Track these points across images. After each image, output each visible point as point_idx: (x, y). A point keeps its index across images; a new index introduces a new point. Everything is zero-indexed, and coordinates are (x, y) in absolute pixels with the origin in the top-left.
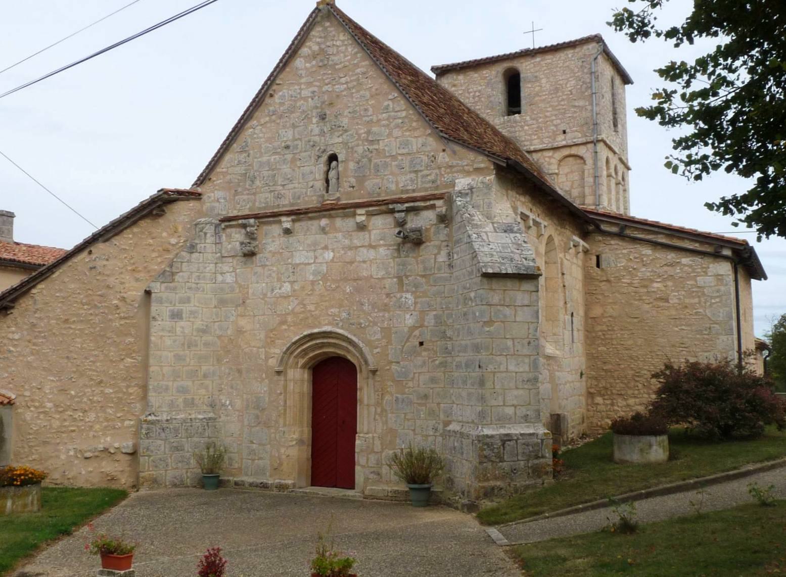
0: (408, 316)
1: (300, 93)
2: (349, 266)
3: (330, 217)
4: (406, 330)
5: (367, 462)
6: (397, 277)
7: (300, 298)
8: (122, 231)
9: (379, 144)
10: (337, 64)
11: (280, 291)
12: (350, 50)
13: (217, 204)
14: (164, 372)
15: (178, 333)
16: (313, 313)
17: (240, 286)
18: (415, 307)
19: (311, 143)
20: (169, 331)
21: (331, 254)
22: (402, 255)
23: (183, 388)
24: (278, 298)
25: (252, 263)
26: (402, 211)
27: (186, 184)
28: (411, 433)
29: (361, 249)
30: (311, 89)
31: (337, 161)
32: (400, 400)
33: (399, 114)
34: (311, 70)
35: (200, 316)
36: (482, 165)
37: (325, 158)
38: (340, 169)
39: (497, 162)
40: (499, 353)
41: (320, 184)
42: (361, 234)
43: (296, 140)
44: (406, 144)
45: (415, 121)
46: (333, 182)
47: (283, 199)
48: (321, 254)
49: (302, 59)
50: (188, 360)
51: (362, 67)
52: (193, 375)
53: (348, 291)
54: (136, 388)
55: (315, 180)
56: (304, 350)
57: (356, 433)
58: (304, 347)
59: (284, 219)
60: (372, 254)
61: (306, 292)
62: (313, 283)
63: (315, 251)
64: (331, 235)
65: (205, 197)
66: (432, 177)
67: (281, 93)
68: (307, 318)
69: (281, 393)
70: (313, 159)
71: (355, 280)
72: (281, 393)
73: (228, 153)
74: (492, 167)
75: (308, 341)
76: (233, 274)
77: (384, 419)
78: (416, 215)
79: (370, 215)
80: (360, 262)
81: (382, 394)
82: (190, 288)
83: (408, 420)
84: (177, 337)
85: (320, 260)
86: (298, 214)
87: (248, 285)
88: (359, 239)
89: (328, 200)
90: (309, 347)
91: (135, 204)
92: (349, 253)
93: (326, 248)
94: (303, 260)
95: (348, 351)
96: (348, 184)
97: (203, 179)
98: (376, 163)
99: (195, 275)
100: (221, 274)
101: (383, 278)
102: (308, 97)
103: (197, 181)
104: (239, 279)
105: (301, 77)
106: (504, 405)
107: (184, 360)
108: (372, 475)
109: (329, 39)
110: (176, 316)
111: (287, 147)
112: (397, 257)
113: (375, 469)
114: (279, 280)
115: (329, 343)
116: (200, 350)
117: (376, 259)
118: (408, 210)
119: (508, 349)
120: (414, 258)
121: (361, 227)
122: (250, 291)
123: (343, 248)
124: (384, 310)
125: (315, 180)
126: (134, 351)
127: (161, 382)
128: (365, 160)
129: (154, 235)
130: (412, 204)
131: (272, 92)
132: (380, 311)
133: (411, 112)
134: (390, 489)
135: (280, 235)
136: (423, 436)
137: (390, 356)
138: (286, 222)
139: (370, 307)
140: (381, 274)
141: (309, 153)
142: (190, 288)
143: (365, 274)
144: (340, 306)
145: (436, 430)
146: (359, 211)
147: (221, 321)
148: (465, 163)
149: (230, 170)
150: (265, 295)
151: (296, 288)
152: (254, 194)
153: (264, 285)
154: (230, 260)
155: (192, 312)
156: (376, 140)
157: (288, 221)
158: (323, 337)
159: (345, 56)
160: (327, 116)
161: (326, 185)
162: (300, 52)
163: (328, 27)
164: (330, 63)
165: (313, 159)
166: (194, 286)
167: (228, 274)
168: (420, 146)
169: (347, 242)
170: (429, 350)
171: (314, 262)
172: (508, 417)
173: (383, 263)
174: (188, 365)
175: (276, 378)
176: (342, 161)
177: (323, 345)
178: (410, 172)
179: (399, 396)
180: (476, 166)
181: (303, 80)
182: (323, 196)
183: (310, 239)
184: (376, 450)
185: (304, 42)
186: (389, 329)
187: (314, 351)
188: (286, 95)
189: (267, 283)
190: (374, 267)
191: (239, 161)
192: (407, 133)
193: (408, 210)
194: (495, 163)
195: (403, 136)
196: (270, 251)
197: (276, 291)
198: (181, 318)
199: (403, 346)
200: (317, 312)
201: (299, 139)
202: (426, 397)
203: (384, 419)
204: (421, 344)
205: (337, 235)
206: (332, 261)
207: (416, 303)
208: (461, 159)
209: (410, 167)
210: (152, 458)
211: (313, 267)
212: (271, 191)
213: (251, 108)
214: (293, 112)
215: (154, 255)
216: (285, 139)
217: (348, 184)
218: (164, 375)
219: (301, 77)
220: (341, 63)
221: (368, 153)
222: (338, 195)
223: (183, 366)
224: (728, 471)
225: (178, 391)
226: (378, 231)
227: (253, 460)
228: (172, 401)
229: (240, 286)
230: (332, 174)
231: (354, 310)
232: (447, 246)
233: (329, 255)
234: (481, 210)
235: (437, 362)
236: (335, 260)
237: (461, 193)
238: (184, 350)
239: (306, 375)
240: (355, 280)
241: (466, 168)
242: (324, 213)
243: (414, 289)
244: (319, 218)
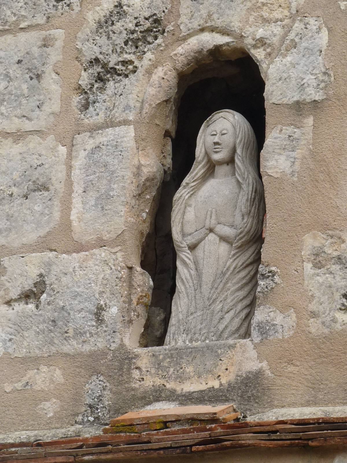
31: (255, 114)
37: (152, 82)
38: (277, 161)
41: (101, 275)
46: (205, 263)
55: (61, 239)
70: (52, 84)
89: (158, 395)
125: (61, 239)
141: (28, 41)
161: (144, 281)
165: (52, 84)
172: (153, 359)
176: (299, 108)
182: (125, 361)
222: (246, 358)
224: (323, 430)
230: (206, 206)
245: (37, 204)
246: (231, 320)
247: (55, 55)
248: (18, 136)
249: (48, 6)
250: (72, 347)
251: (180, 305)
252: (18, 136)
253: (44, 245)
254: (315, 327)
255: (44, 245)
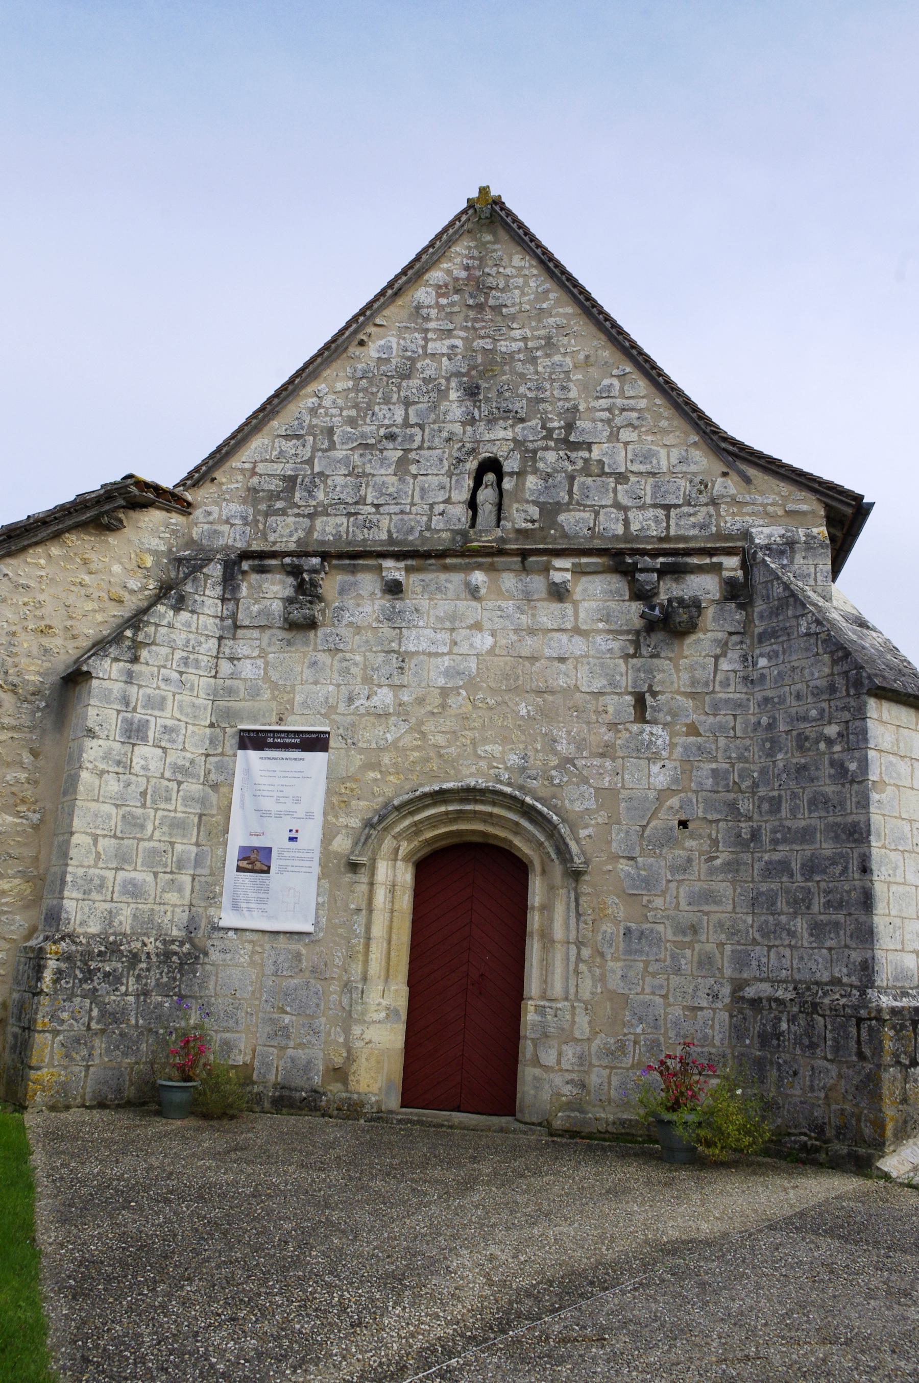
0: (655, 769)
1: (425, 348)
2: (527, 663)
3: (491, 569)
4: (652, 795)
5: (559, 1062)
6: (631, 693)
7: (413, 720)
8: (24, 549)
9: (590, 451)
10: (506, 306)
11: (367, 704)
12: (532, 284)
13: (226, 528)
14: (100, 849)
15: (137, 769)
16: (443, 751)
17: (275, 686)
18: (671, 753)
19: (445, 434)
20: (119, 763)
21: (489, 641)
22: (644, 652)
23: (135, 885)
24: (362, 715)
25: (307, 644)
26: (653, 570)
27: (168, 478)
28: (659, 1000)
29: (556, 635)
30: (448, 342)
32: (636, 934)
33: (632, 402)
34: (448, 310)
35: (181, 737)
36: (805, 507)
37: (472, 465)
39: (834, 503)
40: (893, 847)
42: (555, 607)
43: (412, 426)
44: (646, 457)
45: (667, 419)
47: (375, 529)
48: (467, 638)
49: (430, 290)
50: (150, 827)
51: (558, 315)
52: (153, 859)
53: (523, 712)
54: (17, 881)
56: (415, 824)
57: (523, 999)
58: (417, 818)
59: (388, 563)
60: (578, 646)
61: (429, 708)
62: (445, 692)
63: (452, 630)
64: (490, 604)
65: (198, 513)
66: (700, 518)
67: (382, 342)
68: (428, 760)
69: (359, 910)
71: (540, 692)
72: (359, 910)
73: (260, 435)
74: (822, 513)
75: (427, 807)
76: (260, 662)
77: (598, 971)
78: (676, 580)
79: (579, 571)
80: (550, 659)
81: (594, 921)
82: (166, 680)
83: (654, 975)
84: (133, 778)
85: (464, 648)
86: (419, 556)
87: (293, 686)
88: (549, 614)
90: (428, 818)
91: (67, 496)
92: (529, 640)
93: (477, 626)
94: (423, 646)
95: (517, 829)
96: (523, 515)
97: (201, 476)
98: (583, 483)
99: (179, 654)
100: (231, 659)
101: (601, 694)
102: (443, 355)
103: (186, 479)
104: (271, 672)
105: (427, 319)
106: (902, 950)
107: (142, 827)
108: (569, 1087)
109: (490, 263)
110: (134, 733)
111: (391, 437)
112: (634, 656)
113: (574, 1076)
114: (367, 680)
115: (475, 812)
116: (175, 811)
117: (586, 656)
118: (663, 572)
119: (902, 838)
120: (670, 659)
121: (559, 593)
122: (298, 699)
123: (516, 631)
124: (603, 755)
126: (23, 801)
127: (92, 871)
128: (560, 477)
129: (93, 567)
130: (670, 560)
131: (364, 338)
132: (593, 755)
133: (658, 401)
134: (611, 1118)
135: (373, 593)
136: (685, 1008)
137: (614, 844)
138: (393, 569)
139: (572, 747)
140: (598, 684)
142: (166, 680)
143: (562, 682)
144: (505, 740)
145: (716, 996)
146: (558, 563)
147: (222, 754)
148: (770, 501)
149: (261, 468)
150: (333, 708)
151: (405, 699)
152: (311, 516)
153: (331, 688)
154: (256, 633)
155: (167, 730)
156: (584, 442)
157: (398, 569)
158: (463, 801)
159: (523, 294)
160: (482, 391)
161: (470, 512)
162: (426, 277)
163: (489, 242)
164: (491, 302)
166: (175, 676)
167: (248, 661)
168: (674, 461)
169: (525, 620)
170: (701, 836)
171: (450, 653)
173: (602, 665)
174: (151, 838)
175: (349, 877)
177: (460, 816)
178: (655, 506)
179: (633, 926)
180: (790, 507)
181: (432, 325)
183: (444, 607)
184: (577, 1035)
185: (438, 261)
186: (613, 792)
187: (435, 827)
188: (395, 346)
189: (338, 686)
190: (583, 672)
191: (281, 452)
192: (649, 438)
193: (663, 572)
194: (827, 507)
195: (640, 441)
196: (351, 624)
197: (357, 703)
198: (145, 739)
199: (644, 827)
200: (452, 750)
201: (417, 424)
202: (694, 929)
203: (598, 971)
204: (683, 824)
205: (504, 604)
206: (491, 652)
207: (673, 746)
208: (762, 493)
209: (654, 495)
210: (61, 1037)
211: (447, 661)
212: (349, 515)
213: (319, 360)
214: (408, 377)
215: (90, 606)
216: (387, 422)
217: (523, 515)
218: (98, 854)
219: (427, 319)
220: (513, 305)
221: (567, 463)
223: (140, 840)
225: (125, 892)
226: (594, 605)
227: (283, 1048)
228: (110, 912)
229: (275, 686)
231: (536, 750)
232: (742, 642)
233: (483, 641)
234: (812, 583)
235: (718, 862)
236: (497, 651)
237: (769, 549)
238: (144, 806)
239: (406, 876)
240: (540, 692)
241: (770, 509)
242: (480, 560)
243: (669, 719)
244: (468, 569)
245: (442, 492)
246: (494, 523)
247: (446, 455)
248: (437, 475)
249: (361, 910)
250: (452, 527)
251: (479, 519)
252: (437, 475)
253: (444, 502)
254: (517, 526)
255: (444, 502)
